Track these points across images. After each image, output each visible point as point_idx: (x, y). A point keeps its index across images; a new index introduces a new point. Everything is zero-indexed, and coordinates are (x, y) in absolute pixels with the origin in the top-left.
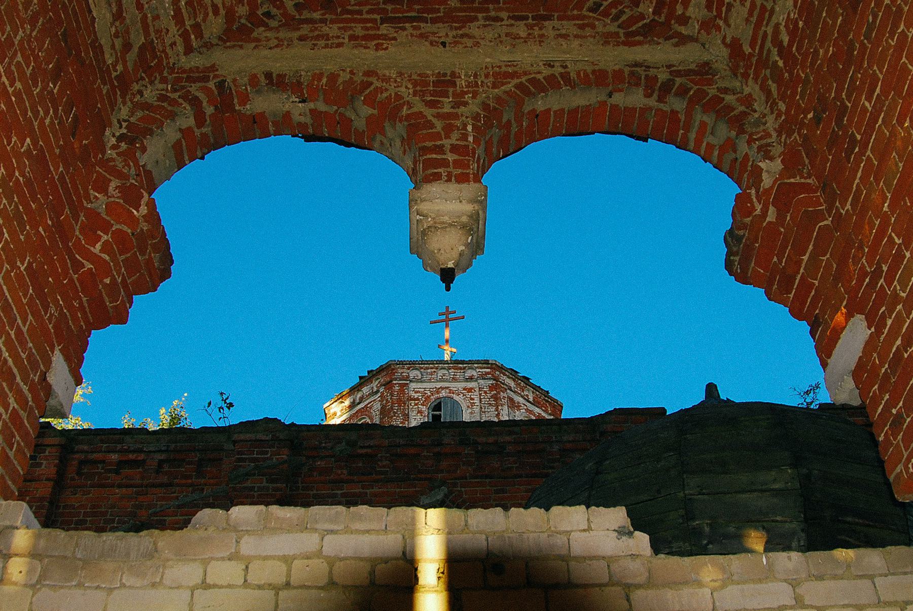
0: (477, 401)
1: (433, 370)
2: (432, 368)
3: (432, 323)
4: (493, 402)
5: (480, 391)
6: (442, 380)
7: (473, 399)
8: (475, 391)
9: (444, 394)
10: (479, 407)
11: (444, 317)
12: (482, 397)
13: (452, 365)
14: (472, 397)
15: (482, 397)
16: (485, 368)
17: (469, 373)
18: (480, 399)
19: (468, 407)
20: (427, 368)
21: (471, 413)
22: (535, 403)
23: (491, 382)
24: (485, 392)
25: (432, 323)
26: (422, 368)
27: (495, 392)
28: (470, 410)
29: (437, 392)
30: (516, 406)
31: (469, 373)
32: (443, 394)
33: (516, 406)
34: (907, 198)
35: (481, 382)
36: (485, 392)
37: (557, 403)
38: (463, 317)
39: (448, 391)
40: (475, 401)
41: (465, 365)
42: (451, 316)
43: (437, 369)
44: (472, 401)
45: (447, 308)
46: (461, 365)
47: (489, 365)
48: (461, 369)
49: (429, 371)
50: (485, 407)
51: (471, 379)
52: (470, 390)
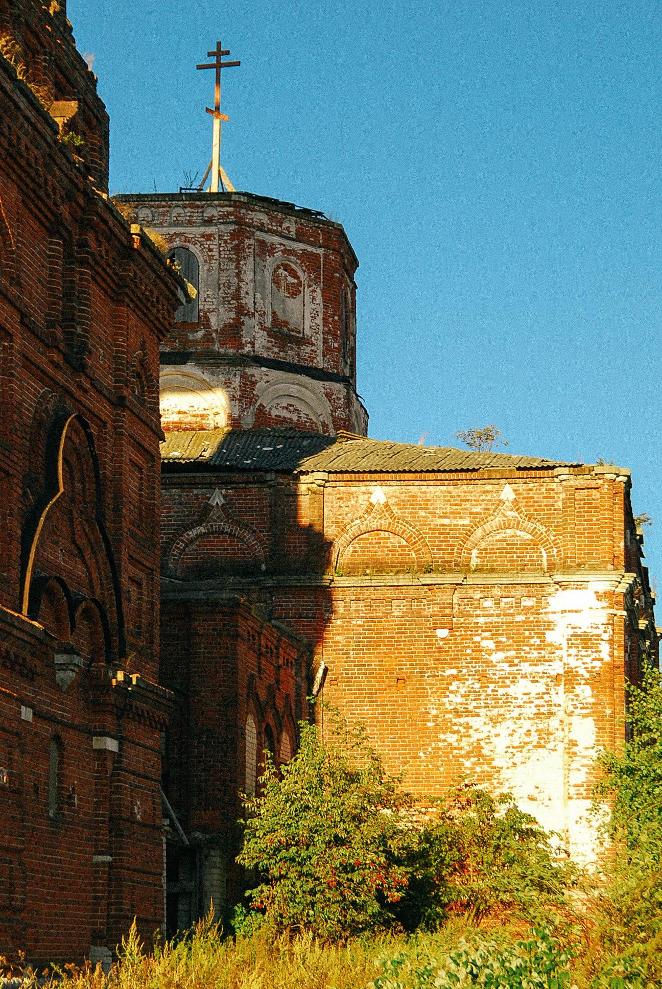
0: (215, 253)
1: (165, 209)
2: (164, 207)
3: (199, 67)
4: (234, 256)
5: (220, 239)
6: (175, 224)
7: (211, 250)
8: (215, 238)
9: (178, 242)
10: (217, 262)
11: (213, 60)
12: (221, 249)
13: (187, 202)
14: (211, 247)
15: (221, 249)
16: (227, 206)
17: (210, 212)
18: (220, 252)
19: (206, 261)
20: (159, 207)
21: (209, 270)
22: (300, 237)
23: (232, 227)
24: (226, 242)
25: (199, 67)
26: (152, 206)
27: (237, 242)
28: (206, 267)
29: (171, 240)
30: (268, 251)
31: (210, 212)
32: (177, 243)
33: (268, 251)
34: (108, 858)
35: (222, 227)
36: (226, 242)
37: (333, 227)
38: (238, 64)
39: (183, 238)
40: (214, 254)
41: (203, 203)
42: (224, 59)
43: (170, 207)
44: (210, 254)
45: (219, 44)
46: (198, 203)
47: (232, 203)
48: (198, 207)
49: (161, 210)
50: (224, 263)
51: (209, 222)
52: (208, 237)
